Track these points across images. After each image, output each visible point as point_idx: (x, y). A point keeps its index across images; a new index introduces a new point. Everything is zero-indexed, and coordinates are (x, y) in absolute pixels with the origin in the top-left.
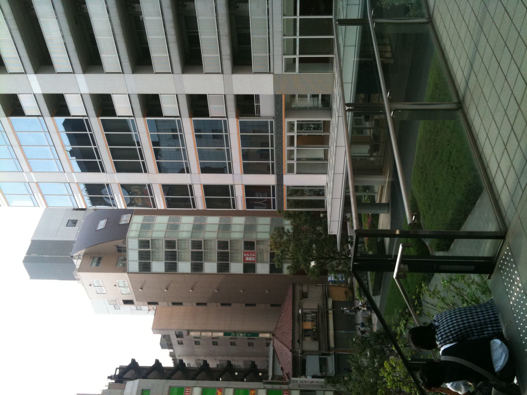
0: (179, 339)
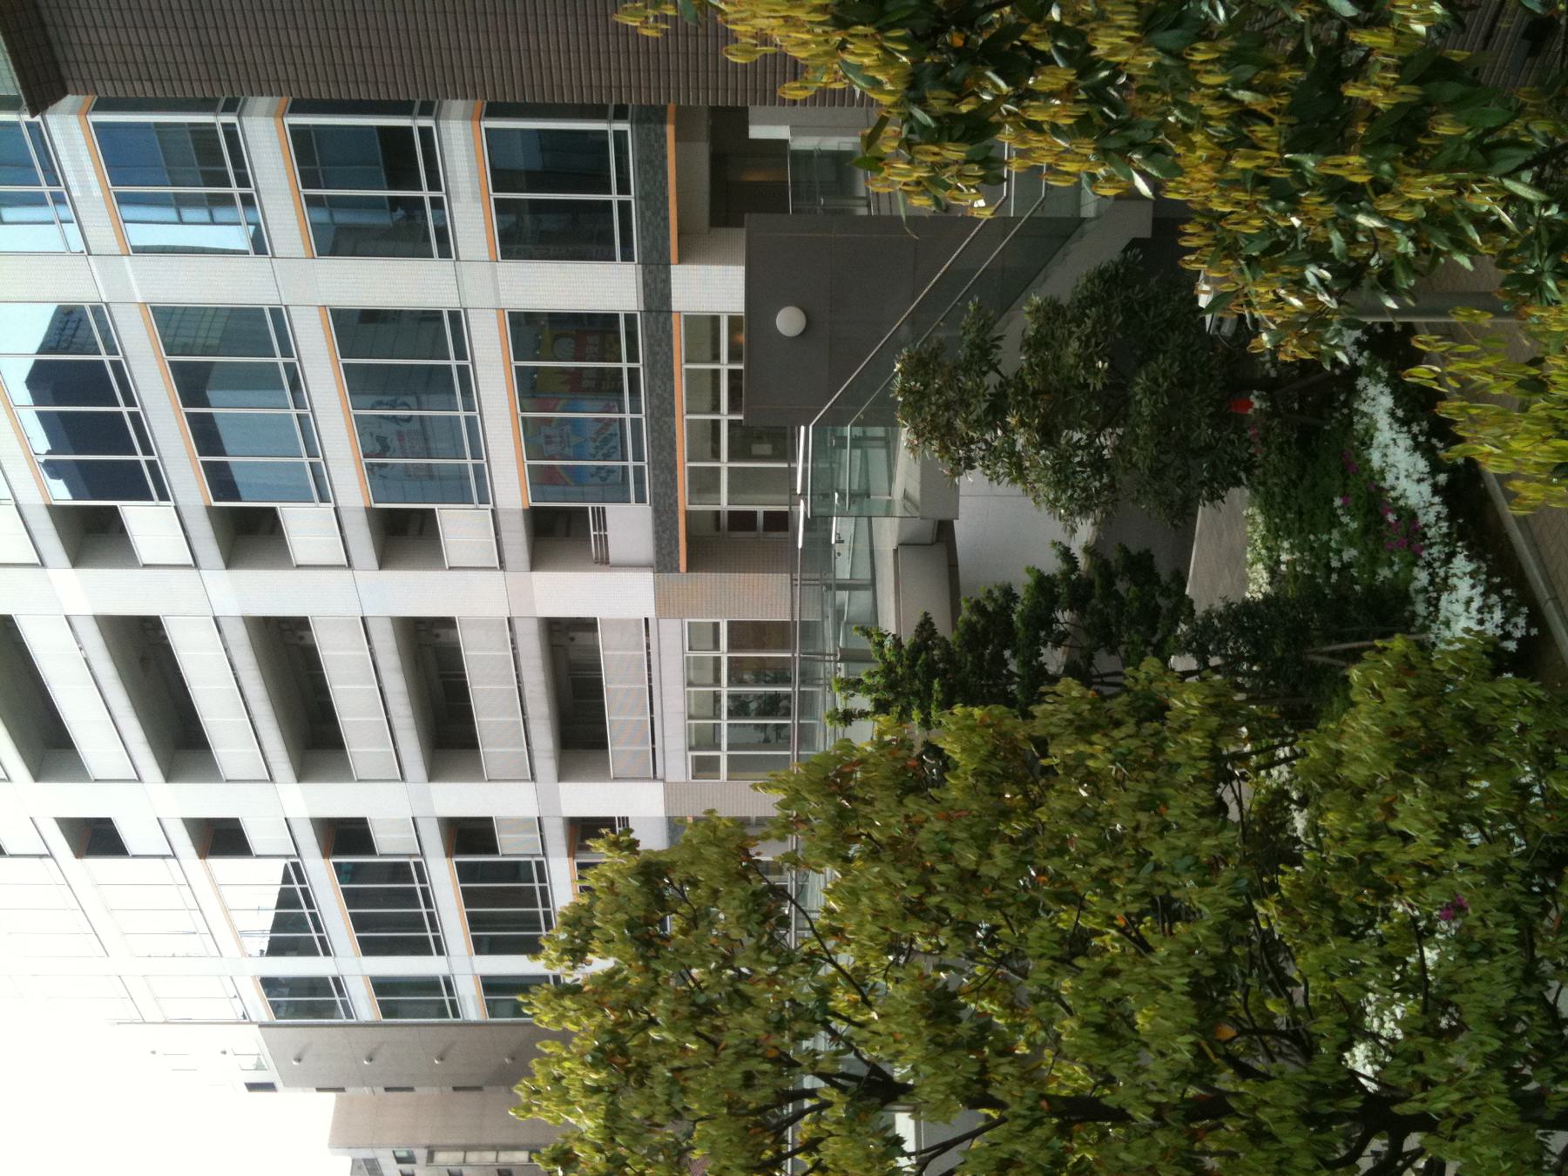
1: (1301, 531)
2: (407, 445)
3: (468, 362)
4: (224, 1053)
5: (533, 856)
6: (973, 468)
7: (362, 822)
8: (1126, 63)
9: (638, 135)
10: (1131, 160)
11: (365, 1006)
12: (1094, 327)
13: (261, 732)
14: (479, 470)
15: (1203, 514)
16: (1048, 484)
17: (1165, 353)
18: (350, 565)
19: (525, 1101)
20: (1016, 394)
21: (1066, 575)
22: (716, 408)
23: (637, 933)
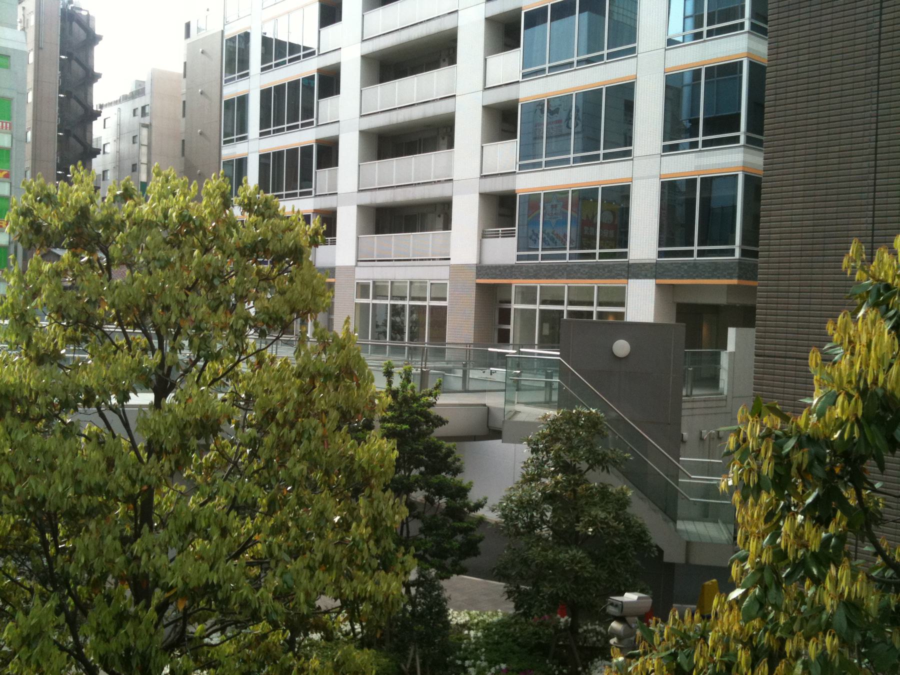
0: (139, 112)
1: (487, 643)
2: (554, 126)
3: (601, 160)
4: (208, 10)
5: (315, 189)
6: (532, 452)
7: (337, 92)
8: (824, 588)
9: (732, 263)
10: (755, 587)
11: (232, 90)
12: (612, 527)
13: (390, 36)
14: (539, 165)
15: (500, 586)
16: (521, 496)
17: (596, 568)
18: (485, 89)
19: (163, 172)
20: (575, 480)
21: (467, 505)
22: (571, 303)
23: (259, 245)
